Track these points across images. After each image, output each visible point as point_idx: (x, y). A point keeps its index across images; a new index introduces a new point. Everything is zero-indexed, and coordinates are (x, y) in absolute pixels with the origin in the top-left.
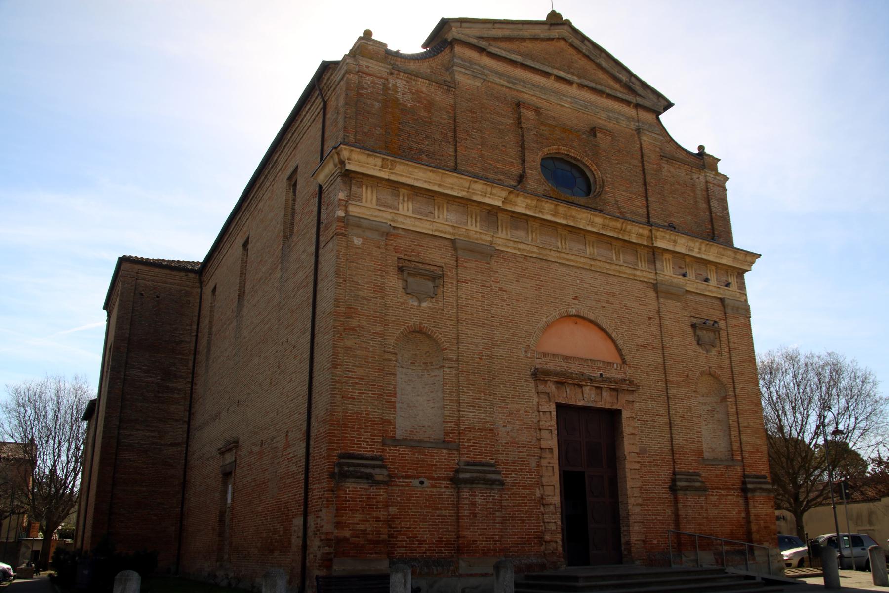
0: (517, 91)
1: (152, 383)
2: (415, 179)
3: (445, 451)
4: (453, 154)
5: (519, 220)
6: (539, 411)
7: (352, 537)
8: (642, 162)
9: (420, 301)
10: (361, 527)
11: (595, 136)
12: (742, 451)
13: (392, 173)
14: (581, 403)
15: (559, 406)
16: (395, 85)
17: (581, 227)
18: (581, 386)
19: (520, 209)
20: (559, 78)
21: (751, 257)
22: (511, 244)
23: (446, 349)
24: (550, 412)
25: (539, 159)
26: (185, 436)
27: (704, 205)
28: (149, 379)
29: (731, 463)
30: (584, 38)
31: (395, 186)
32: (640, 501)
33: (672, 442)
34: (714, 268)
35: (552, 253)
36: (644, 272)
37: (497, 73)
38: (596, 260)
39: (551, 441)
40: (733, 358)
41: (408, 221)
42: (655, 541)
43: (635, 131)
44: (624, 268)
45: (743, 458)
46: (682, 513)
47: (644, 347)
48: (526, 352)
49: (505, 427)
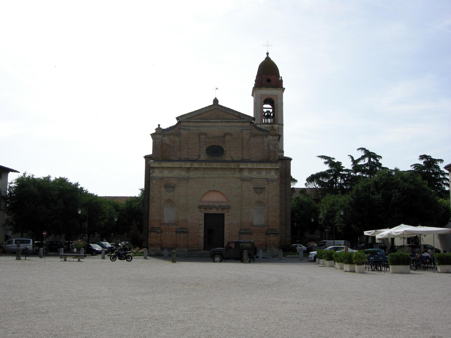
0: (200, 130)
3: (175, 226)
5: (196, 169)
9: (170, 193)
16: (165, 139)
17: (215, 167)
24: (202, 216)
25: (205, 148)
31: (163, 168)
32: (228, 236)
36: (237, 175)
38: (220, 175)
39: (202, 222)
47: (235, 196)
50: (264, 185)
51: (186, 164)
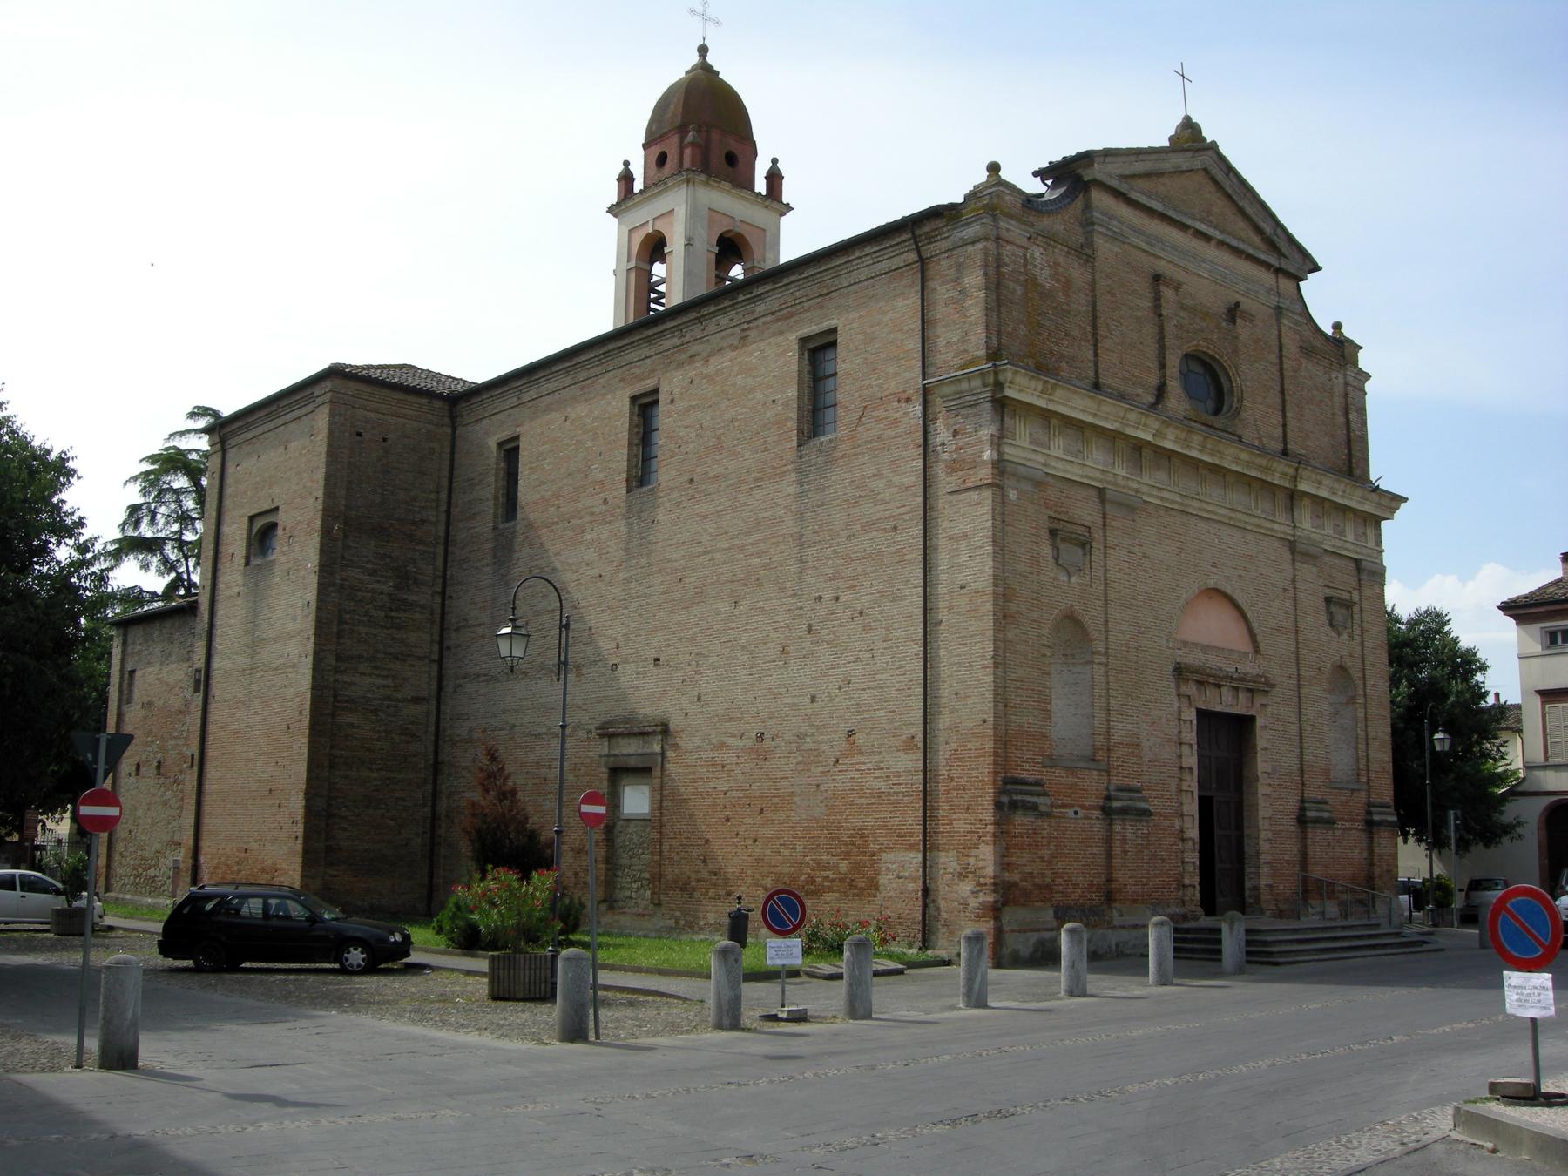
1: (382, 593)
2: (1072, 407)
3: (1095, 773)
4: (1092, 358)
5: (1165, 457)
6: (1180, 720)
7: (1021, 881)
8: (1281, 357)
10: (1028, 869)
11: (1234, 323)
12: (1368, 770)
13: (1050, 400)
14: (1219, 708)
15: (1201, 714)
18: (1219, 686)
19: (1169, 445)
20: (1200, 234)
21: (1394, 501)
22: (1155, 492)
23: (1095, 640)
24: (1191, 721)
26: (434, 687)
27: (1342, 420)
28: (377, 586)
29: (1356, 787)
30: (1230, 170)
33: (1302, 758)
34: (1351, 515)
35: (1194, 503)
36: (1281, 525)
37: (1139, 232)
40: (1366, 644)
41: (1060, 465)
42: (1281, 888)
43: (1274, 309)
44: (1262, 520)
45: (1368, 779)
46: (1310, 852)
48: (1167, 640)
49: (1148, 740)
50: (1349, 592)
51: (1145, 425)
